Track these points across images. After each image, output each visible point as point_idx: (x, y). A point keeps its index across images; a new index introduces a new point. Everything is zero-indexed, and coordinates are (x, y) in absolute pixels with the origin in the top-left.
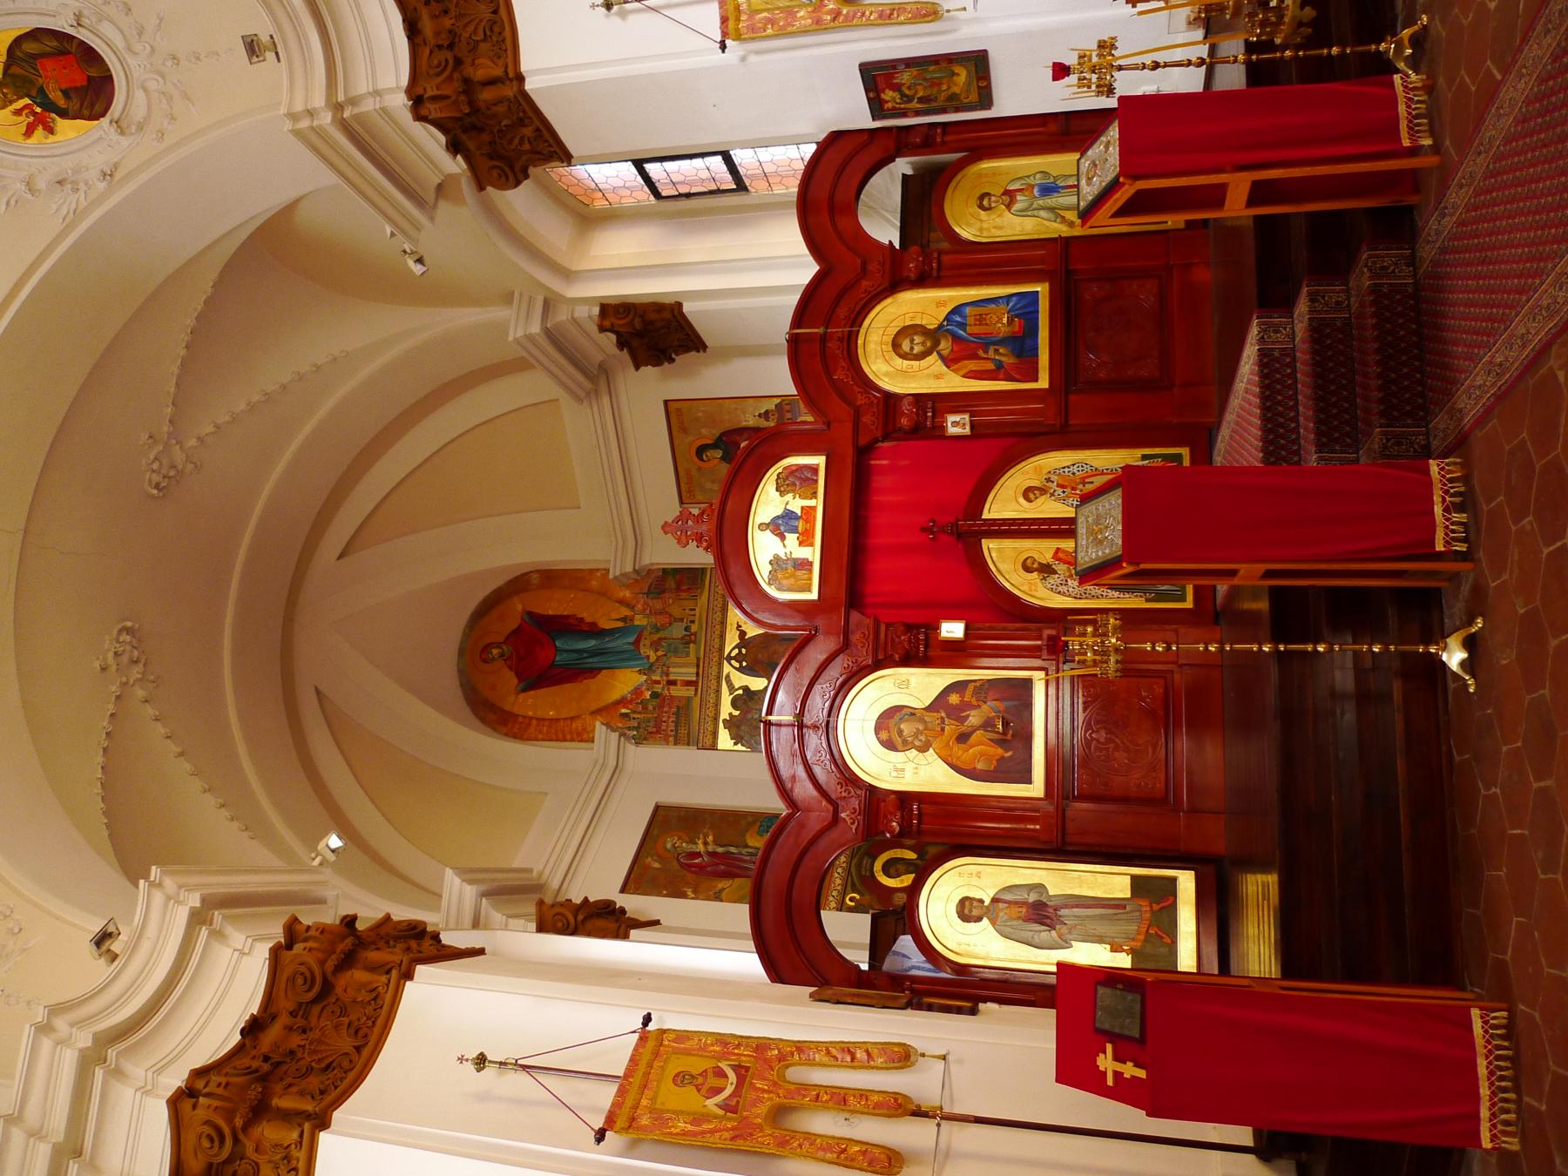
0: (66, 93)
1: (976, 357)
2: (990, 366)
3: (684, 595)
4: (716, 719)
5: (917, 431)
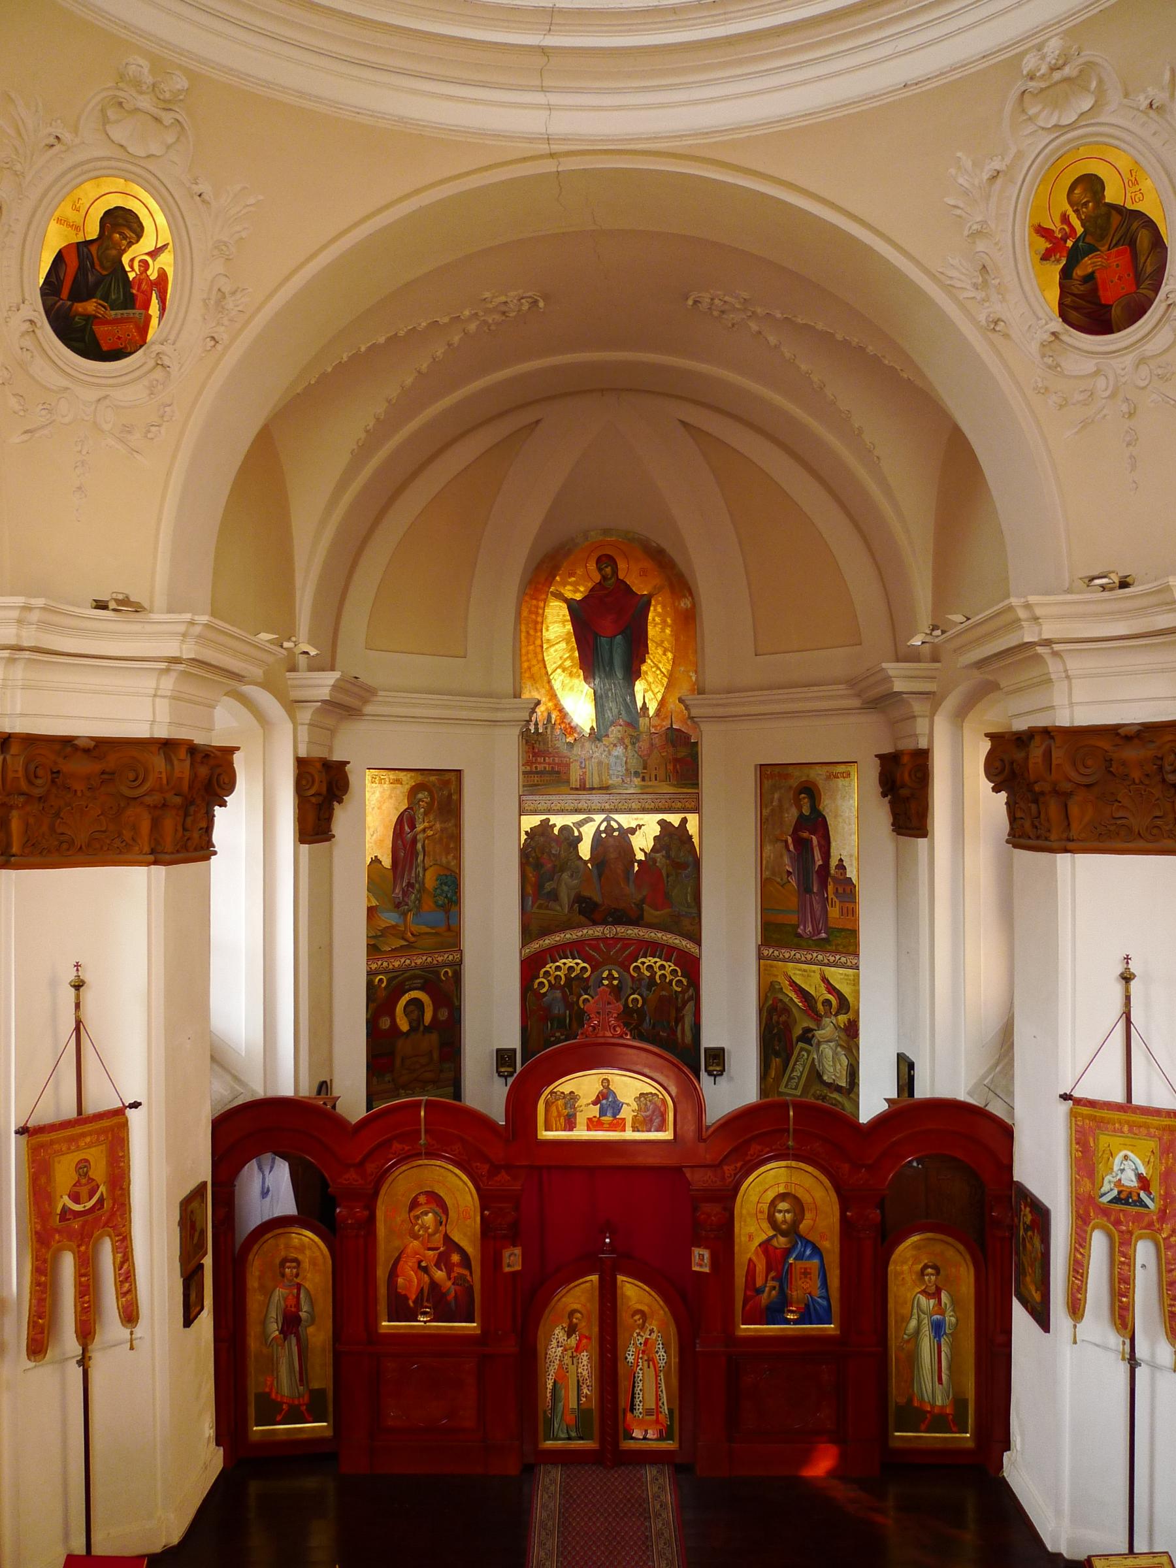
0: (1089, 278)
1: (769, 1269)
2: (759, 1282)
3: (670, 767)
4: (549, 811)
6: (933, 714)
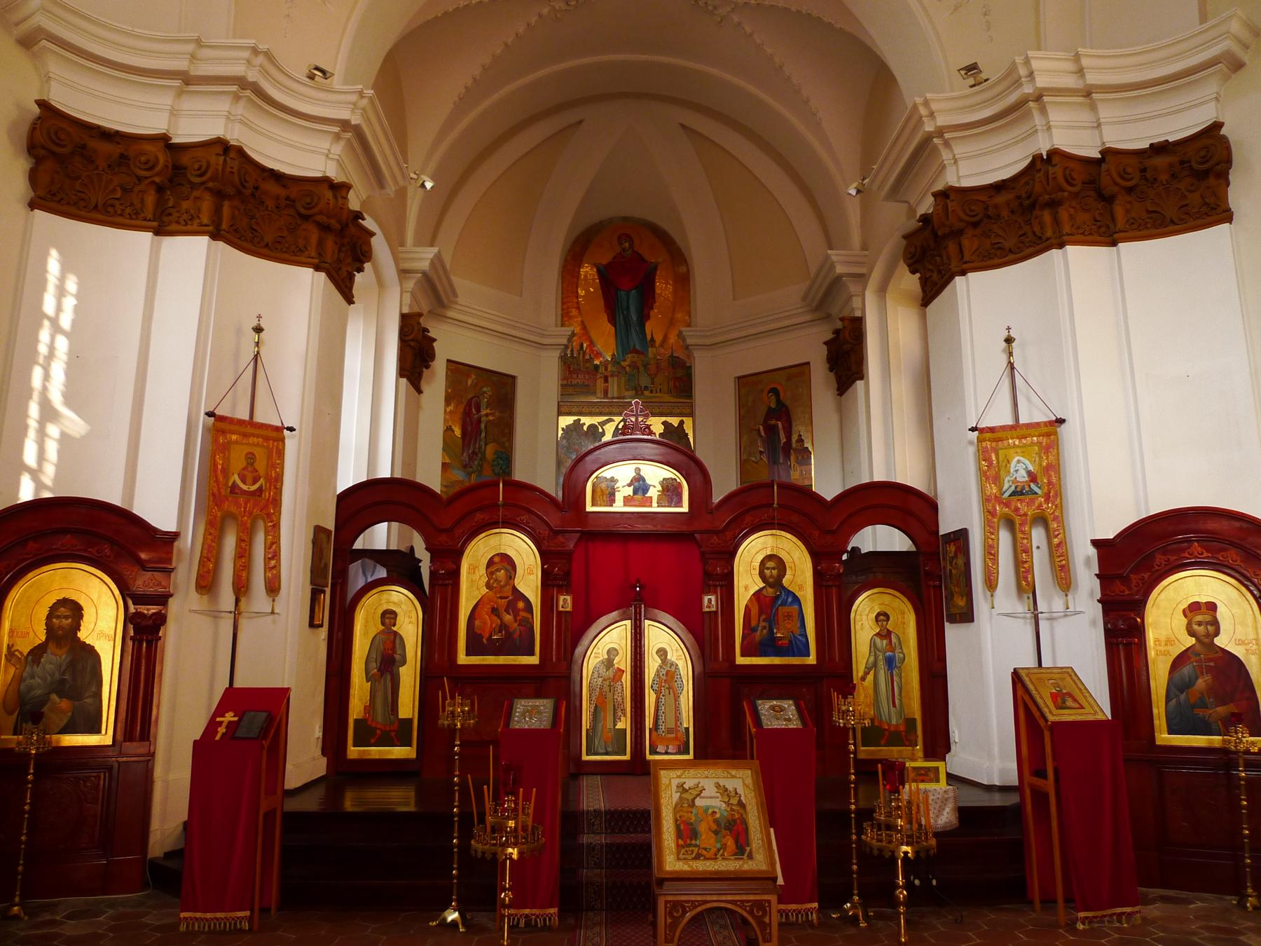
1: (761, 612)
2: (753, 623)
3: (672, 384)
5: (708, 575)
6: (864, 290)
